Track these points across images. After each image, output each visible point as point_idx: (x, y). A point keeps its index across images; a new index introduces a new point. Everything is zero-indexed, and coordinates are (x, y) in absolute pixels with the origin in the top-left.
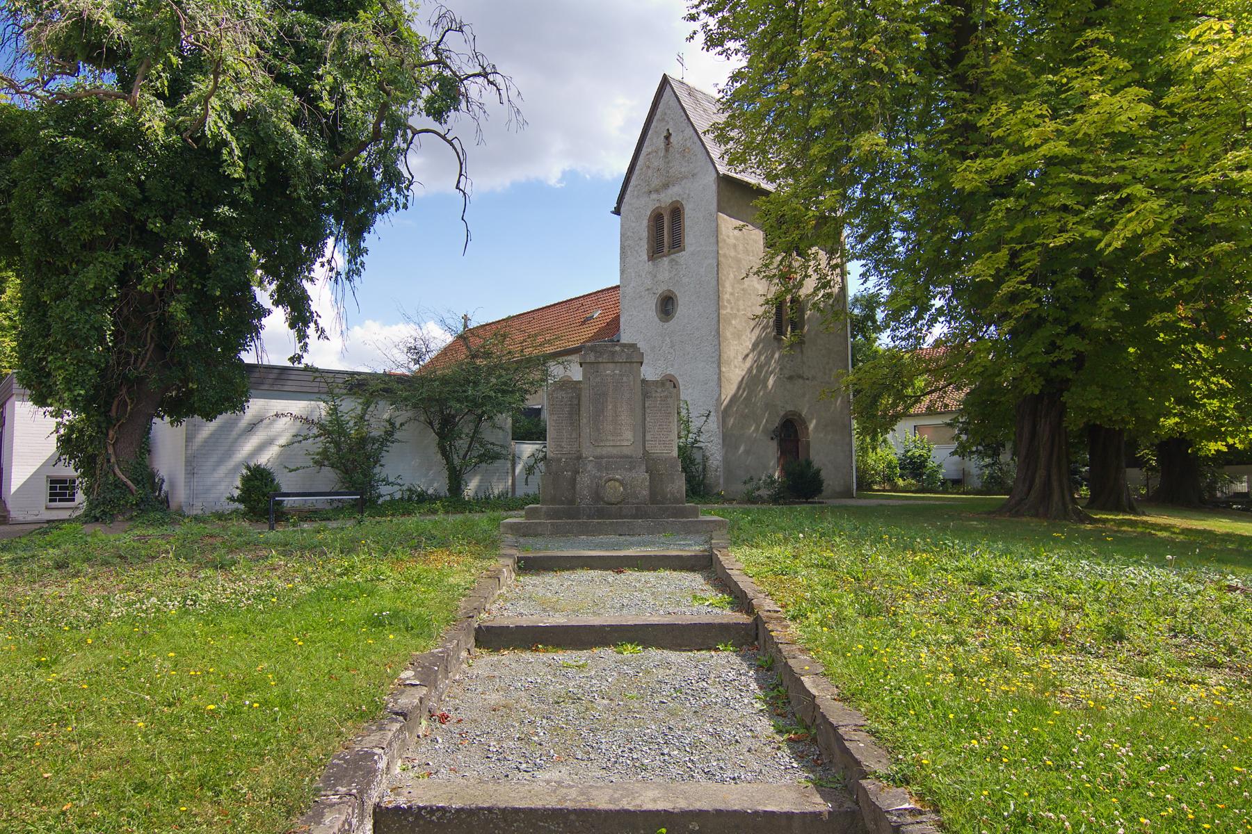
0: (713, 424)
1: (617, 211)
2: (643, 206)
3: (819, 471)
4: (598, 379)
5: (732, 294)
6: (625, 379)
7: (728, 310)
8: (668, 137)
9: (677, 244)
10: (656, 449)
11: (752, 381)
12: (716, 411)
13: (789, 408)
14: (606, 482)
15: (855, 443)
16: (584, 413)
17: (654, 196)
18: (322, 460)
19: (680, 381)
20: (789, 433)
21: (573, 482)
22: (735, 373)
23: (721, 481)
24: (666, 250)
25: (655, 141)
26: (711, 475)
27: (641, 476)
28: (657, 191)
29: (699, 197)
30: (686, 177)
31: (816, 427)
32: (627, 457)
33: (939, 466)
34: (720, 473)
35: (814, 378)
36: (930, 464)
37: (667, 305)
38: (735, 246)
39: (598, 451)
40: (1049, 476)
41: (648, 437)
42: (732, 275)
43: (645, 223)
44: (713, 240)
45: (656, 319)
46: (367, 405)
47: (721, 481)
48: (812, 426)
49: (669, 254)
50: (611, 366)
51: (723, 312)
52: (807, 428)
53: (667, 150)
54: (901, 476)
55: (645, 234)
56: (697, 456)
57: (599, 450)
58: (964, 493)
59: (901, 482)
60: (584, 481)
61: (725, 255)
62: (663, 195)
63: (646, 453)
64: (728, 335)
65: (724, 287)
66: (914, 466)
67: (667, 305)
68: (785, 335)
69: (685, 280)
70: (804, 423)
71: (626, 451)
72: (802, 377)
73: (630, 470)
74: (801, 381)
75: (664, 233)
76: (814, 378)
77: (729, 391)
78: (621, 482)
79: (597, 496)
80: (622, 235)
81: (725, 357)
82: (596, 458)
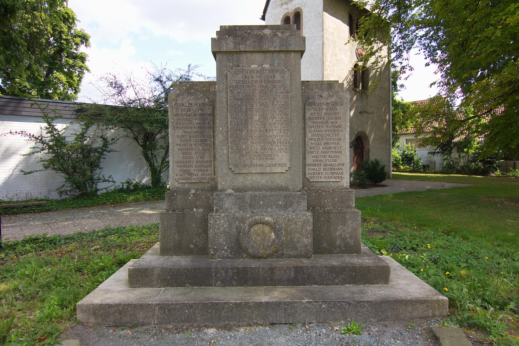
3: (383, 168)
4: (239, 77)
5: (330, 62)
6: (278, 77)
7: (328, 72)
10: (321, 177)
13: (360, 129)
14: (251, 226)
16: (220, 128)
17: (285, 6)
18: (49, 165)
21: (204, 223)
27: (301, 218)
31: (374, 139)
32: (280, 189)
33: (420, 159)
36: (416, 158)
38: (333, 33)
39: (240, 181)
41: (310, 160)
44: (321, 29)
46: (87, 126)
48: (371, 140)
50: (258, 57)
51: (325, 72)
52: (368, 141)
54: (402, 165)
57: (241, 179)
58: (434, 173)
59: (402, 167)
60: (220, 224)
62: (290, 5)
63: (306, 181)
66: (408, 159)
68: (359, 88)
70: (367, 138)
71: (280, 181)
72: (366, 112)
73: (285, 207)
74: (366, 114)
76: (373, 113)
78: (273, 227)
79: (238, 248)
82: (237, 190)
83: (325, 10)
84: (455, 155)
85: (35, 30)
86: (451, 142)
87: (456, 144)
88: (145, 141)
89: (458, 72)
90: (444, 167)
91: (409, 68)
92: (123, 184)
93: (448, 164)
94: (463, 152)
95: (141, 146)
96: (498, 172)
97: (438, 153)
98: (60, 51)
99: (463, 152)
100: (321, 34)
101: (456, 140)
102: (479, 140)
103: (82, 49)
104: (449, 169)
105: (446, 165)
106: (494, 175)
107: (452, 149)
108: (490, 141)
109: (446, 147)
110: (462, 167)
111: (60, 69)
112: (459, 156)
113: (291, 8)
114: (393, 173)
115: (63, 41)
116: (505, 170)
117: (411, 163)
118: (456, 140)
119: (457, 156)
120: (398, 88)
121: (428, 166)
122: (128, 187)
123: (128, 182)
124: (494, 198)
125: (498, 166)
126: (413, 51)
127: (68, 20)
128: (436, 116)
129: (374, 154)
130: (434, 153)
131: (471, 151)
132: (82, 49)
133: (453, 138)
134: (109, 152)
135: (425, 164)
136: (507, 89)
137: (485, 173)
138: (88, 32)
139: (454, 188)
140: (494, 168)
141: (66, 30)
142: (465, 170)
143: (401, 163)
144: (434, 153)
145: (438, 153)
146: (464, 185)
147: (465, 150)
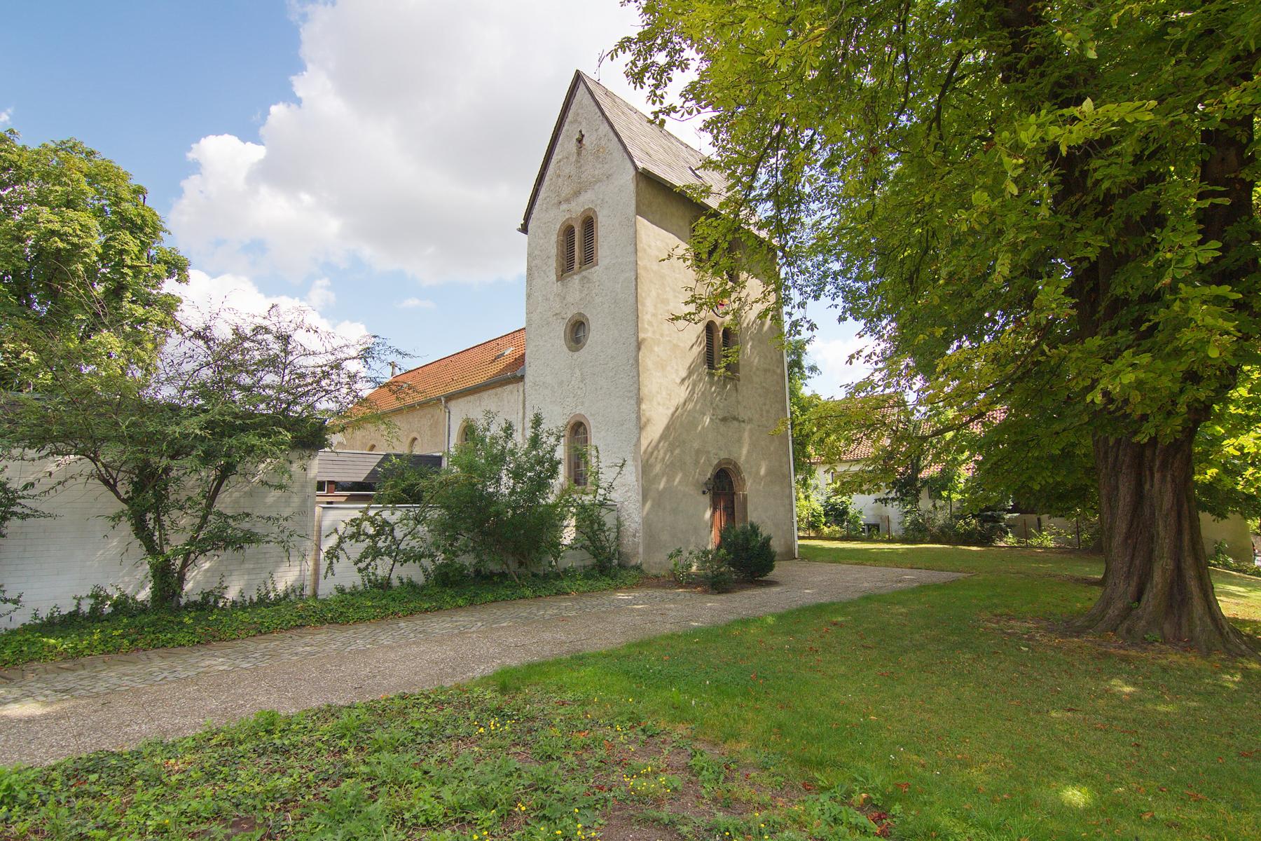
0: (631, 476)
1: (524, 229)
2: (551, 220)
3: (769, 539)
5: (654, 315)
8: (580, 141)
9: (589, 258)
11: (677, 429)
12: (635, 459)
13: (723, 455)
15: (794, 494)
17: (564, 207)
19: (591, 422)
20: (723, 486)
22: (659, 413)
23: (641, 550)
24: (576, 266)
25: (567, 145)
26: (627, 542)
28: (567, 200)
29: (614, 198)
30: (600, 181)
33: (860, 512)
34: (639, 539)
35: (750, 420)
36: (851, 511)
37: (577, 331)
40: (1179, 569)
42: (654, 293)
43: (554, 238)
44: (630, 249)
45: (565, 348)
47: (641, 550)
49: (579, 272)
53: (579, 154)
55: (554, 251)
56: (609, 519)
59: (826, 530)
61: (645, 268)
64: (650, 364)
65: (643, 305)
67: (577, 331)
69: (598, 300)
72: (737, 419)
75: (577, 246)
76: (750, 420)
77: (654, 432)
80: (529, 255)
81: (645, 391)
83: (639, 212)
84: (925, 503)
85: (61, 245)
86: (917, 479)
87: (925, 482)
88: (139, 487)
89: (918, 346)
90: (907, 529)
91: (806, 325)
92: (80, 599)
93: (914, 523)
94: (941, 497)
95: (124, 501)
96: (1010, 539)
97: (893, 499)
98: (117, 292)
99: (941, 497)
100: (632, 259)
101: (924, 474)
102: (965, 473)
103: (170, 286)
104: (917, 532)
105: (911, 523)
106: (1003, 544)
107: (918, 491)
108: (989, 472)
109: (908, 488)
110: (941, 529)
111: (116, 324)
112: (934, 506)
113: (576, 209)
114: (800, 542)
115: (126, 270)
116: (1023, 534)
117: (843, 521)
118: (924, 474)
119: (930, 506)
120: (807, 373)
121: (877, 526)
122: (94, 610)
123: (95, 596)
124: (1011, 618)
125: (1009, 526)
126: (825, 300)
127: (141, 230)
128: (871, 427)
129: (759, 510)
130: (885, 501)
131: (956, 497)
132: (170, 286)
133: (919, 471)
134: (24, 517)
135: (872, 521)
136: (1010, 368)
137: (984, 539)
138: (183, 252)
139: (923, 588)
140: (1002, 529)
141: (136, 250)
142: (945, 535)
143: (824, 520)
144: (885, 501)
145: (893, 499)
146: (945, 574)
147: (945, 494)
